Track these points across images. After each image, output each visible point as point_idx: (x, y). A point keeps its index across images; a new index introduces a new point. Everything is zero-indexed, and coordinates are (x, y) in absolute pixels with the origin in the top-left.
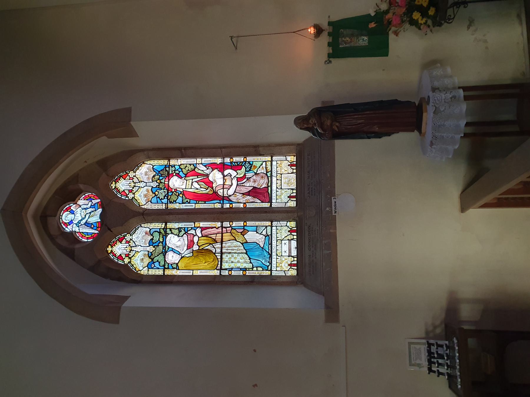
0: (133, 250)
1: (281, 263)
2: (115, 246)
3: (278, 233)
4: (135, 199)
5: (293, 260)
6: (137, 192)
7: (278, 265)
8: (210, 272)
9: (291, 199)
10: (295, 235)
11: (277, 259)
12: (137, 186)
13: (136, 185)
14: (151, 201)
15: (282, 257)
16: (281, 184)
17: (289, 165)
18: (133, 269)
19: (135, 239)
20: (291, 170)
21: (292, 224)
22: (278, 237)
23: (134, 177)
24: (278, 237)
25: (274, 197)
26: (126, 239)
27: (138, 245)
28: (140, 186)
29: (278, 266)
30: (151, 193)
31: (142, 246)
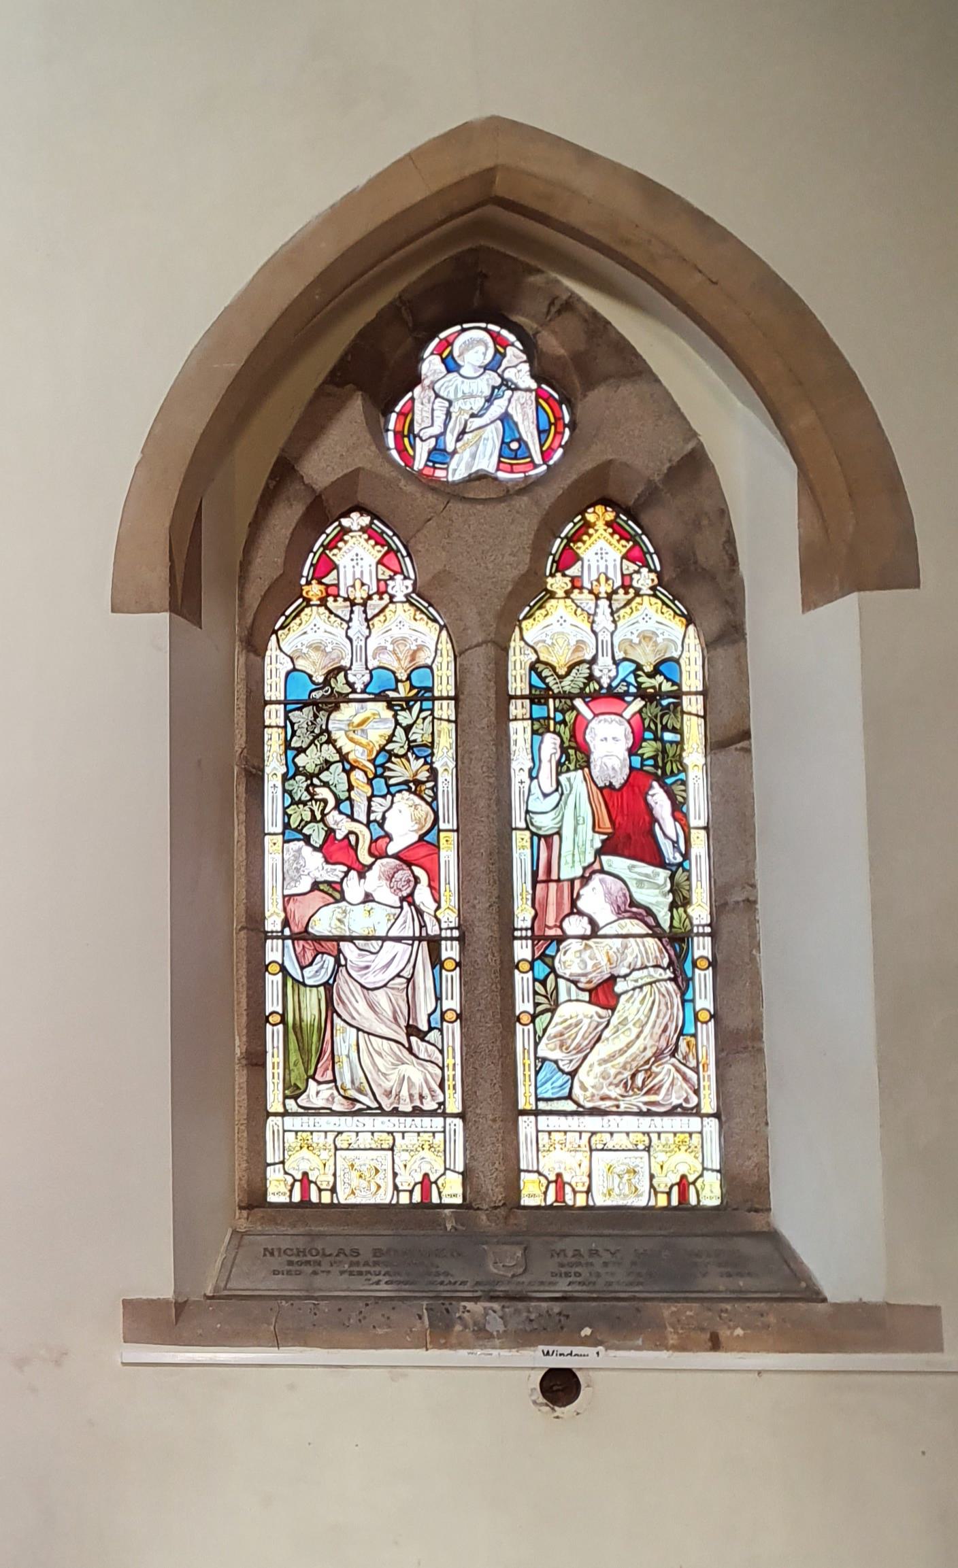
0: (352, 612)
2: (612, 535)
7: (304, 1135)
9: (298, 1185)
12: (597, 606)
13: (604, 603)
14: (294, 669)
15: (333, 1150)
17: (426, 1176)
26: (638, 572)
27: (371, 626)
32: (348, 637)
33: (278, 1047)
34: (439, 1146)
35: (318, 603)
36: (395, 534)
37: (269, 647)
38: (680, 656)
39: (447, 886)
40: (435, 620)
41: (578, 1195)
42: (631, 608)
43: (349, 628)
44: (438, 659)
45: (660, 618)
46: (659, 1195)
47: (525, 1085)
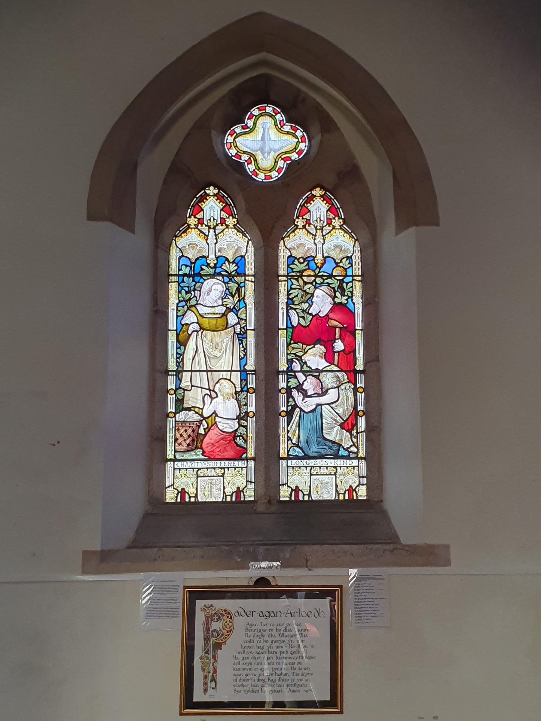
1: (300, 475)
3: (235, 469)
4: (296, 229)
5: (305, 493)
6: (199, 232)
8: (283, 357)
10: (344, 497)
11: (192, 470)
12: (209, 232)
13: (212, 231)
14: (183, 256)
16: (318, 475)
17: (351, 487)
18: (286, 233)
19: (227, 233)
20: (228, 492)
21: (250, 494)
22: (340, 469)
23: (333, 226)
24: (321, 469)
25: (351, 463)
26: (334, 219)
27: (325, 239)
28: (208, 237)
29: (294, 470)
30: (341, 256)
31: (216, 245)
32: (315, 243)
33: (250, 428)
34: (244, 474)
35: (339, 228)
36: (229, 197)
37: (280, 245)
38: (352, 255)
39: (283, 354)
40: (353, 238)
41: (305, 496)
42: (224, 233)
43: (315, 239)
44: (248, 254)
45: (344, 239)
46: (227, 497)
47: (170, 446)
